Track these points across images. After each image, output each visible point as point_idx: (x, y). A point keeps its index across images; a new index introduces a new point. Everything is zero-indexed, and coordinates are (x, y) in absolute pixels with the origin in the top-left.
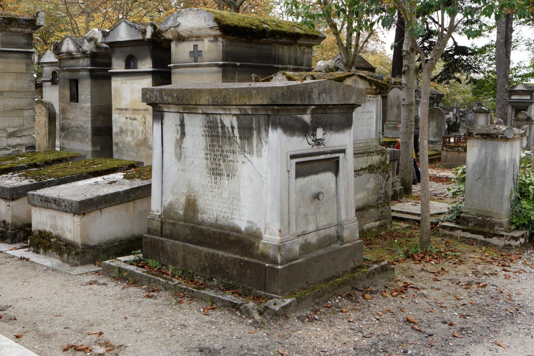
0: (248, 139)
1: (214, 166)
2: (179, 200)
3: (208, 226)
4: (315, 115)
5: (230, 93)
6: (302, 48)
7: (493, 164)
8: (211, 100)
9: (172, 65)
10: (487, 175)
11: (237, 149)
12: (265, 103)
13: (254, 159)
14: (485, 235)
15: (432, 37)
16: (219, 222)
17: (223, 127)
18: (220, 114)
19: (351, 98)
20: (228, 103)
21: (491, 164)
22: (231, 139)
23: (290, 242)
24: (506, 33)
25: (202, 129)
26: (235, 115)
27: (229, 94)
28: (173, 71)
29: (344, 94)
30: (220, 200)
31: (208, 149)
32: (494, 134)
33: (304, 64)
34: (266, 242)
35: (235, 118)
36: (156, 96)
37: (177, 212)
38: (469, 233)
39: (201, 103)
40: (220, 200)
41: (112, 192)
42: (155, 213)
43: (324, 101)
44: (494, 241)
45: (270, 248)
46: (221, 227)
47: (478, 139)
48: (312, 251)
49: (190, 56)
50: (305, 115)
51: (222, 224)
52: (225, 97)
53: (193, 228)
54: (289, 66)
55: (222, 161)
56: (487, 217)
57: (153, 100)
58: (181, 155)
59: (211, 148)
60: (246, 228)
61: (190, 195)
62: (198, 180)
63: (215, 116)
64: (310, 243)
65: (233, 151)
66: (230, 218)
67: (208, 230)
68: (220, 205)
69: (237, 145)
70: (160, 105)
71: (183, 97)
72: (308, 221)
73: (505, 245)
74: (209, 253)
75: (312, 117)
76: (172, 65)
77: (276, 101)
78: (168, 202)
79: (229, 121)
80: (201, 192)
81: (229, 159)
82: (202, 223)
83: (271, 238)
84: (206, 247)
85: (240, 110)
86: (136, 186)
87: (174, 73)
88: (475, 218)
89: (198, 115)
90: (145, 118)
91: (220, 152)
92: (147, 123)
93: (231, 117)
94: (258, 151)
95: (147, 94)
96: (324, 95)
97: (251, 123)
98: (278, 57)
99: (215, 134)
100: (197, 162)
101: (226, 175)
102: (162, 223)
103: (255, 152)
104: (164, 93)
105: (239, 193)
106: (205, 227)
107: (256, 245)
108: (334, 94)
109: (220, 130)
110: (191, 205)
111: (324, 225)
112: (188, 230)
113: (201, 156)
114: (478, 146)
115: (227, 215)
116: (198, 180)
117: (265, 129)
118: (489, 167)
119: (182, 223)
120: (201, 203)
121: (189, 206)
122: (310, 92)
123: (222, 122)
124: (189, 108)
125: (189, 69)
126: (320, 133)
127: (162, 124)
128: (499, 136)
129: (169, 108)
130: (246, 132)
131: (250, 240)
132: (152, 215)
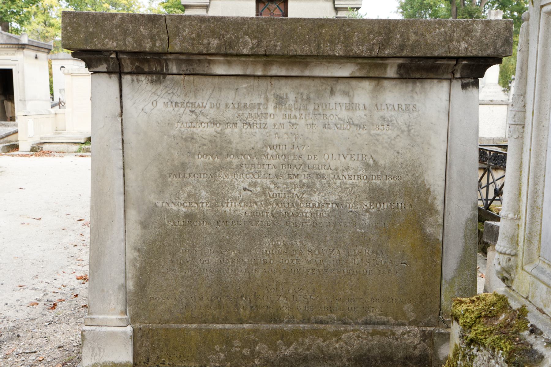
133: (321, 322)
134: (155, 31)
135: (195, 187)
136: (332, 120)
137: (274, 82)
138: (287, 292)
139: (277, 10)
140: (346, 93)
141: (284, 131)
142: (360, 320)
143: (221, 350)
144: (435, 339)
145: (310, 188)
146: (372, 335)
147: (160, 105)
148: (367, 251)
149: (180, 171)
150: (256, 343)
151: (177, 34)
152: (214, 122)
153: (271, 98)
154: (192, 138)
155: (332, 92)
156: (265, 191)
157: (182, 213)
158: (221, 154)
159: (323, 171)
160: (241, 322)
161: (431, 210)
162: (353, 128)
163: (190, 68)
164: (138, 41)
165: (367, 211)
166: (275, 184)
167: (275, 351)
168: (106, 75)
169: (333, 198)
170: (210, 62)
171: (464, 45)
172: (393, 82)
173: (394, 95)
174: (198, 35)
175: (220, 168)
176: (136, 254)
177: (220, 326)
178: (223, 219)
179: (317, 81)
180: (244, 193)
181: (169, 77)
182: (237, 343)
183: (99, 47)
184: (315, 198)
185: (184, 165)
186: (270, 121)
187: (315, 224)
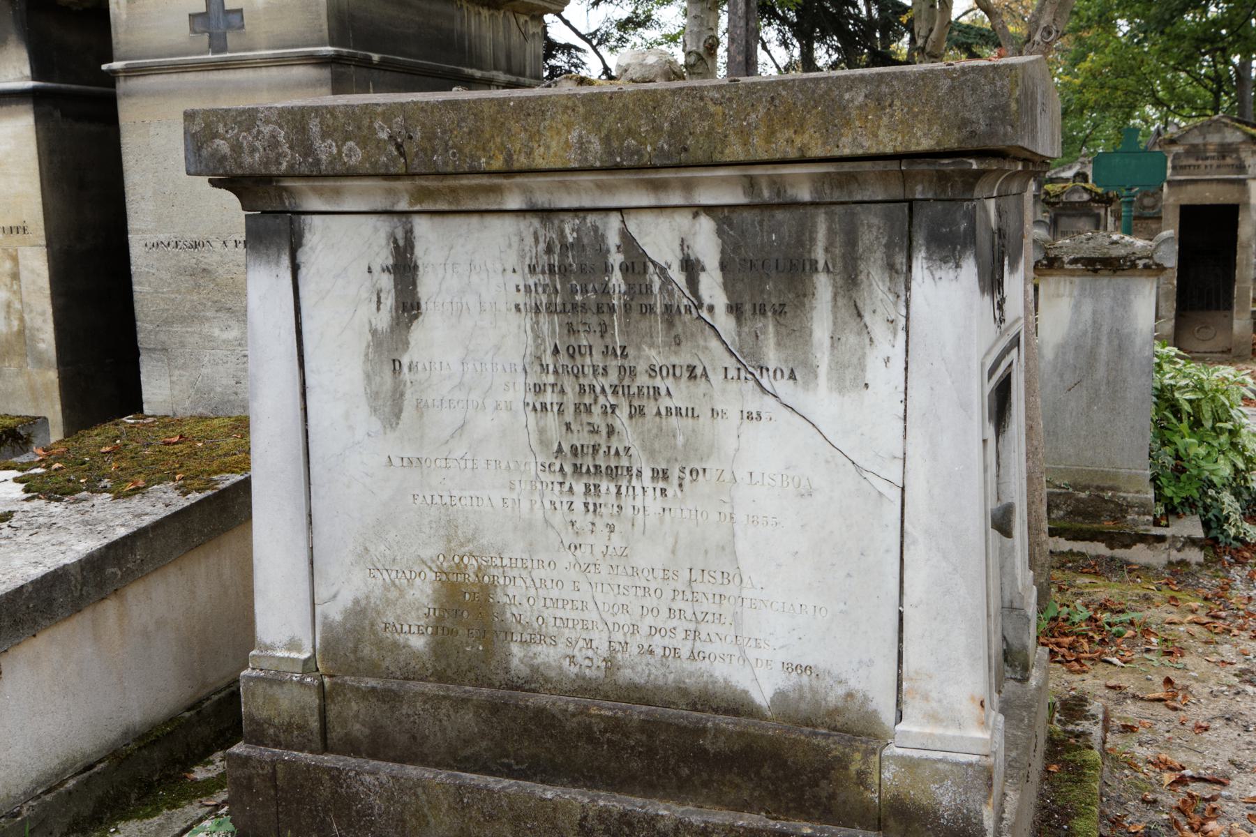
0: (780, 311)
1: (582, 438)
2: (402, 593)
3: (573, 692)
5: (712, 108)
6: (522, 19)
7: (1116, 342)
8: (596, 146)
9: (116, 65)
10: (1101, 372)
11: (714, 356)
12: (925, 144)
13: (821, 400)
14: (1112, 539)
15: (554, 57)
16: (625, 675)
17: (636, 263)
18: (620, 210)
20: (701, 156)
21: (1110, 342)
22: (680, 318)
24: (747, 42)
25: (518, 279)
26: (709, 209)
27: (705, 114)
28: (122, 86)
30: (623, 581)
31: (544, 368)
32: (1125, 258)
33: (528, 73)
34: (916, 754)
35: (706, 225)
36: (274, 143)
37: (395, 644)
38: (1062, 540)
39: (541, 163)
40: (623, 581)
41: (37, 572)
42: (279, 654)
44: (1139, 554)
45: (941, 778)
46: (636, 694)
47: (1072, 273)
49: (193, 30)
51: (640, 680)
52: (677, 130)
53: (495, 708)
54: (494, 73)
55: (623, 412)
56: (1103, 489)
57: (252, 161)
58: (397, 397)
59: (564, 359)
60: (780, 696)
61: (460, 569)
62: (497, 502)
63: (591, 218)
65: (691, 369)
66: (685, 653)
67: (583, 711)
68: (622, 599)
69: (714, 344)
70: (287, 183)
71: (430, 137)
73: (1170, 563)
74: (603, 816)
76: (116, 65)
77: (992, 134)
78: (346, 599)
79: (673, 236)
80: (517, 550)
81: (665, 402)
82: (535, 680)
83: (942, 738)
84: (574, 782)
85: (751, 184)
86: (122, 532)
87: (128, 95)
88: (1069, 496)
89: (495, 222)
90: (15, 259)
91: (613, 377)
92: (24, 274)
93: (683, 221)
94: (839, 367)
95: (216, 135)
97: (800, 243)
98: (470, 41)
99: (586, 294)
100: (485, 423)
101: (647, 474)
102: (324, 695)
103: (823, 371)
104: (314, 126)
105: (728, 549)
106: (561, 701)
107: (854, 768)
109: (617, 280)
110: (468, 608)
112: (467, 718)
113: (509, 396)
114: (1071, 295)
115: (667, 641)
116: (497, 502)
117: (891, 267)
118: (1104, 351)
119: (431, 688)
120: (519, 598)
121: (457, 613)
123: (628, 241)
124: (453, 190)
125: (190, 77)
127: (295, 269)
128: (1141, 263)
129: (337, 193)
130: (769, 278)
131: (817, 749)
132: (265, 665)
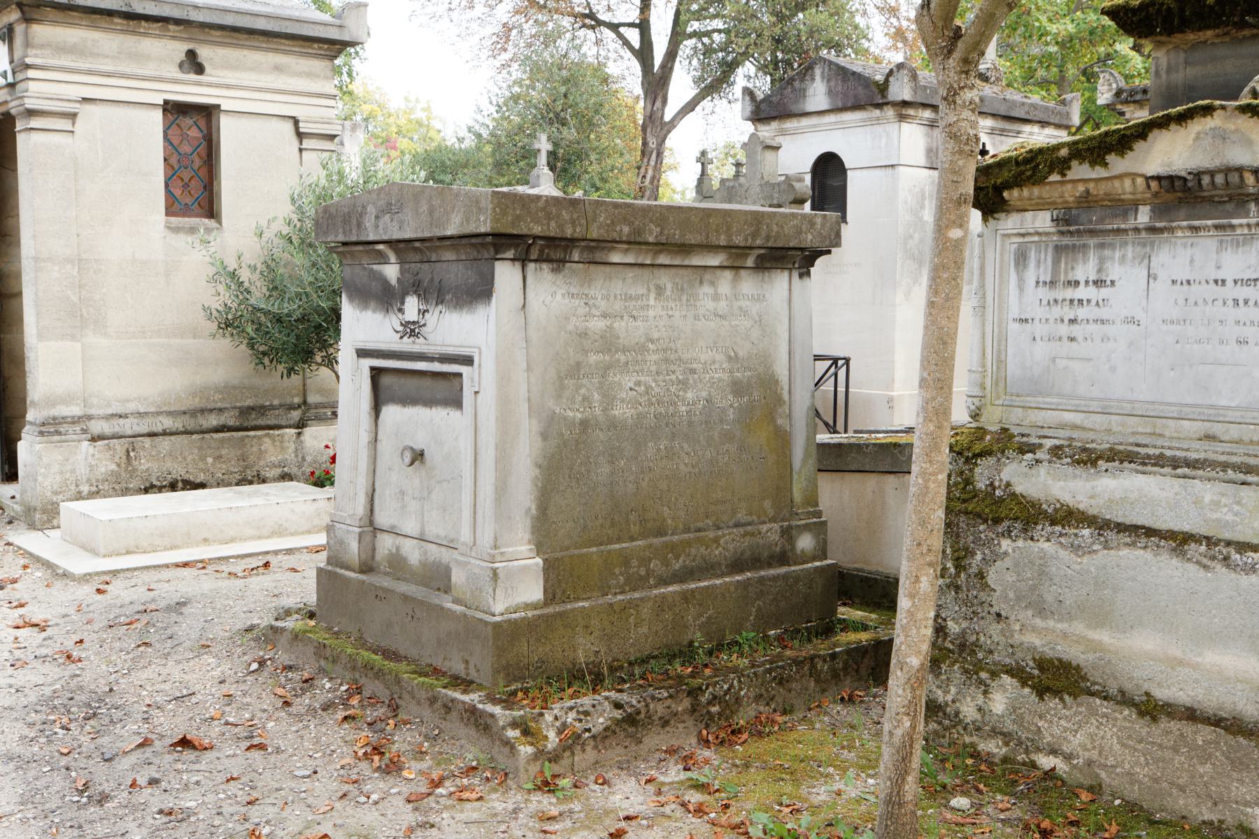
4: (407, 266)
19: (448, 220)
23: (344, 527)
29: (431, 212)
43: (385, 233)
48: (405, 580)
50: (387, 266)
64: (404, 560)
72: (404, 507)
75: (402, 271)
96: (387, 217)
108: (408, 215)
111: (438, 536)
122: (361, 215)
126: (412, 306)
133: (699, 530)
134: (575, 216)
135: (588, 389)
136: (702, 311)
137: (656, 271)
138: (670, 501)
139: (194, 129)
140: (712, 283)
141: (662, 323)
142: (731, 523)
143: (621, 574)
144: (794, 532)
145: (684, 384)
146: (744, 536)
147: (559, 297)
148: (733, 448)
149: (575, 371)
150: (650, 560)
151: (594, 220)
152: (605, 316)
153: (652, 288)
154: (584, 334)
155: (701, 282)
156: (648, 388)
157: (577, 420)
158: (610, 350)
159: (695, 366)
160: (632, 539)
161: (779, 400)
162: (718, 319)
163: (591, 256)
164: (561, 226)
165: (731, 406)
166: (656, 381)
167: (667, 566)
168: (509, 263)
169: (704, 394)
170: (613, 248)
171: (810, 237)
172: (748, 272)
173: (749, 284)
174: (613, 222)
175: (608, 367)
176: (538, 471)
177: (617, 546)
178: (613, 424)
179: (690, 270)
180: (630, 393)
181: (568, 265)
182: (635, 563)
183: (525, 231)
184: (690, 395)
185: (578, 364)
186: (651, 313)
187: (690, 423)
